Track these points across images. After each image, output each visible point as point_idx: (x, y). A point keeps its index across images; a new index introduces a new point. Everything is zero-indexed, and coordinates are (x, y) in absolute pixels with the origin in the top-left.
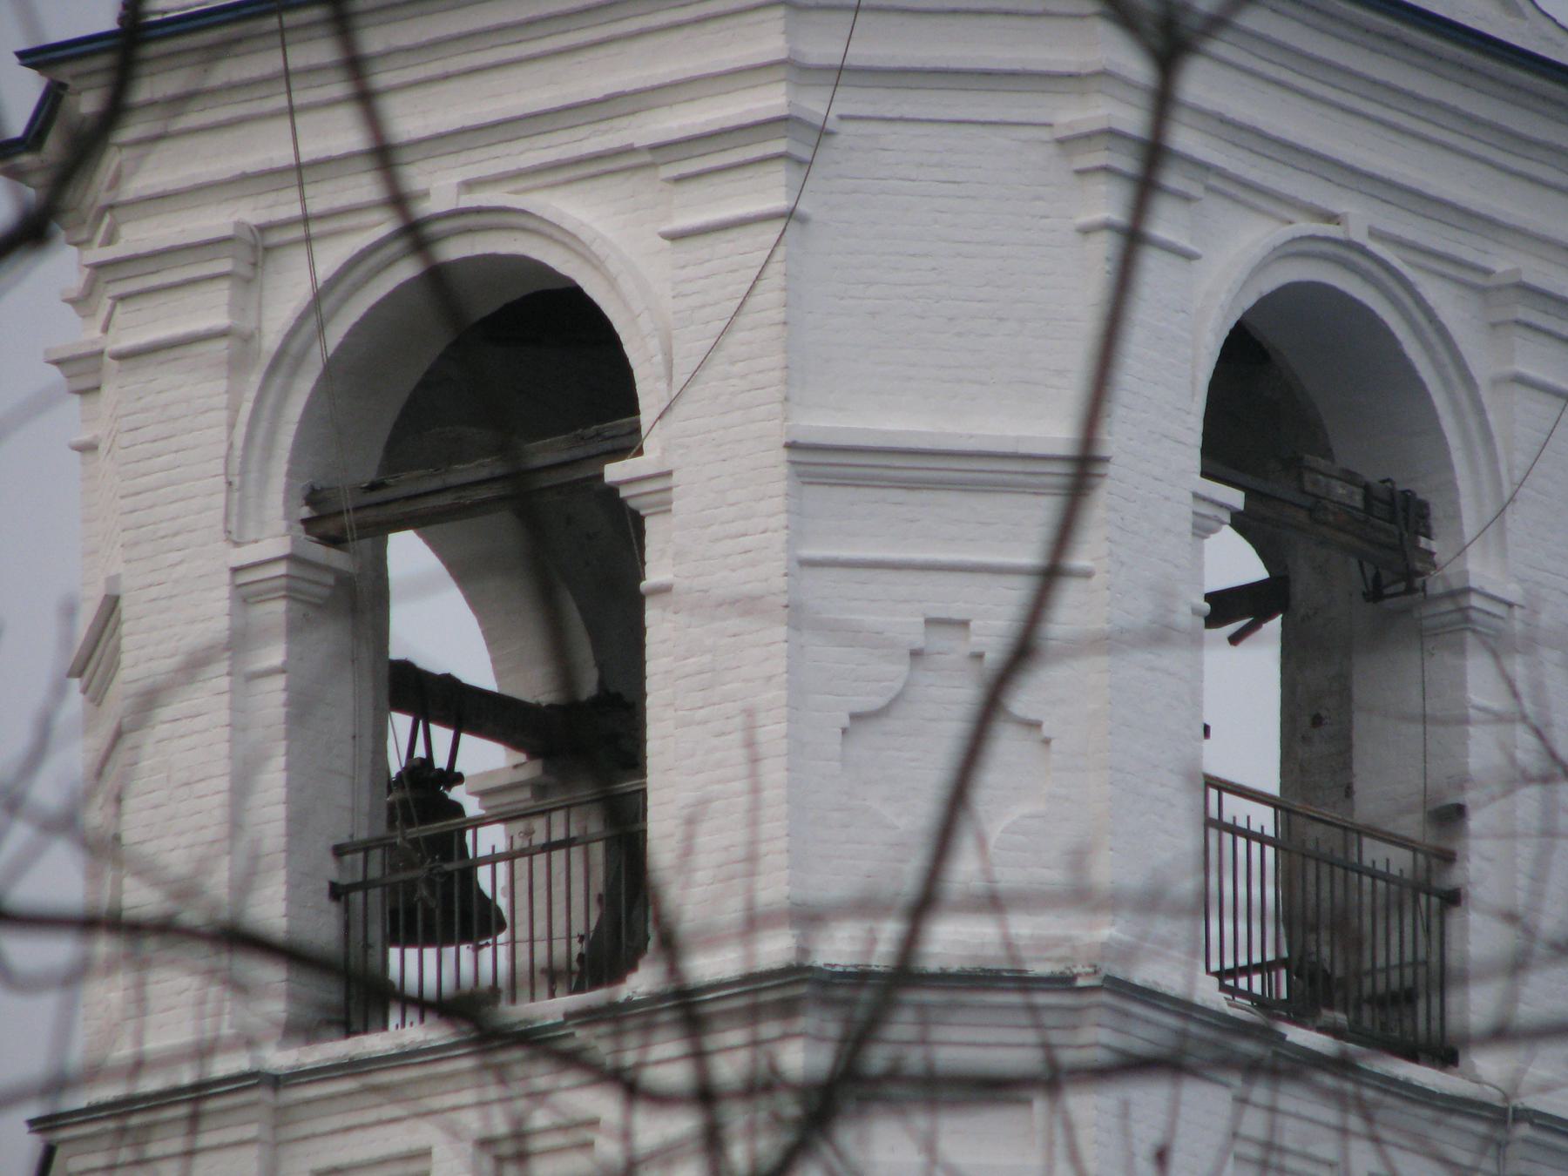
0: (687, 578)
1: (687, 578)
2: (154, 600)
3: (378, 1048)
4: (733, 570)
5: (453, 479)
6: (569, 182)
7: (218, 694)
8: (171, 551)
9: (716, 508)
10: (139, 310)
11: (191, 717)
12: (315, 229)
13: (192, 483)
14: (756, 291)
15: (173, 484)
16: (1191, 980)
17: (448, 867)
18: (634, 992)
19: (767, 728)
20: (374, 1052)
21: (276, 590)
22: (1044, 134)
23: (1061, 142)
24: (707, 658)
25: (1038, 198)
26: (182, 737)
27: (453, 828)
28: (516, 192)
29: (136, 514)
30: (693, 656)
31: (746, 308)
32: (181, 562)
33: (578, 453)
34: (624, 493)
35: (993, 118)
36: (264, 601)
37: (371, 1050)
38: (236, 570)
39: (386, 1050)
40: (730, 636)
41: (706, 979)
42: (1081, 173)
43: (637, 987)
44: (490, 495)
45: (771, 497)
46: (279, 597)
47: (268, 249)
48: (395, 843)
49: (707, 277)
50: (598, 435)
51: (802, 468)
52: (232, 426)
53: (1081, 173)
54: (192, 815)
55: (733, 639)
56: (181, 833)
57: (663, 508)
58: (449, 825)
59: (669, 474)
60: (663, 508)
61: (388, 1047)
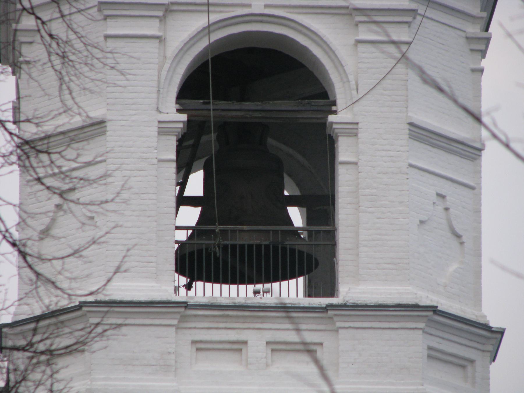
0: (365, 161)
1: (365, 161)
2: (123, 126)
3: (223, 302)
4: (385, 162)
5: (244, 107)
6: (316, 13)
7: (152, 164)
8: (130, 110)
9: (378, 139)
10: (116, 22)
11: (139, 170)
12: (211, 8)
13: (142, 88)
14: (395, 67)
15: (133, 86)
16: (95, 333)
17: (226, 242)
18: (347, 302)
19: (399, 220)
20: (222, 303)
21: (174, 132)
22: (463, 34)
23: (467, 38)
24: (374, 191)
25: (462, 56)
26: (135, 176)
27: (228, 229)
28: (290, 13)
29: (114, 94)
30: (368, 189)
31: (390, 73)
32: (135, 115)
33: (300, 108)
34: (334, 126)
35: (453, 25)
36: (100, 136)
37: (220, 302)
38: (159, 122)
39: (227, 303)
40: (384, 185)
41: (380, 303)
42: (472, 50)
43: (349, 300)
44: (260, 116)
45: (401, 140)
46: (174, 135)
47: (171, 11)
48: (214, 231)
49: (374, 58)
50: (309, 103)
51: (413, 133)
52: (160, 71)
53: (472, 50)
54: (140, 205)
55: (385, 186)
56: (134, 211)
57: (103, 133)
58: (228, 228)
59: (357, 123)
60: (103, 133)
61: (228, 302)
